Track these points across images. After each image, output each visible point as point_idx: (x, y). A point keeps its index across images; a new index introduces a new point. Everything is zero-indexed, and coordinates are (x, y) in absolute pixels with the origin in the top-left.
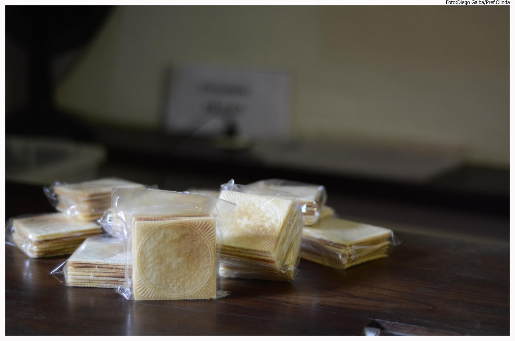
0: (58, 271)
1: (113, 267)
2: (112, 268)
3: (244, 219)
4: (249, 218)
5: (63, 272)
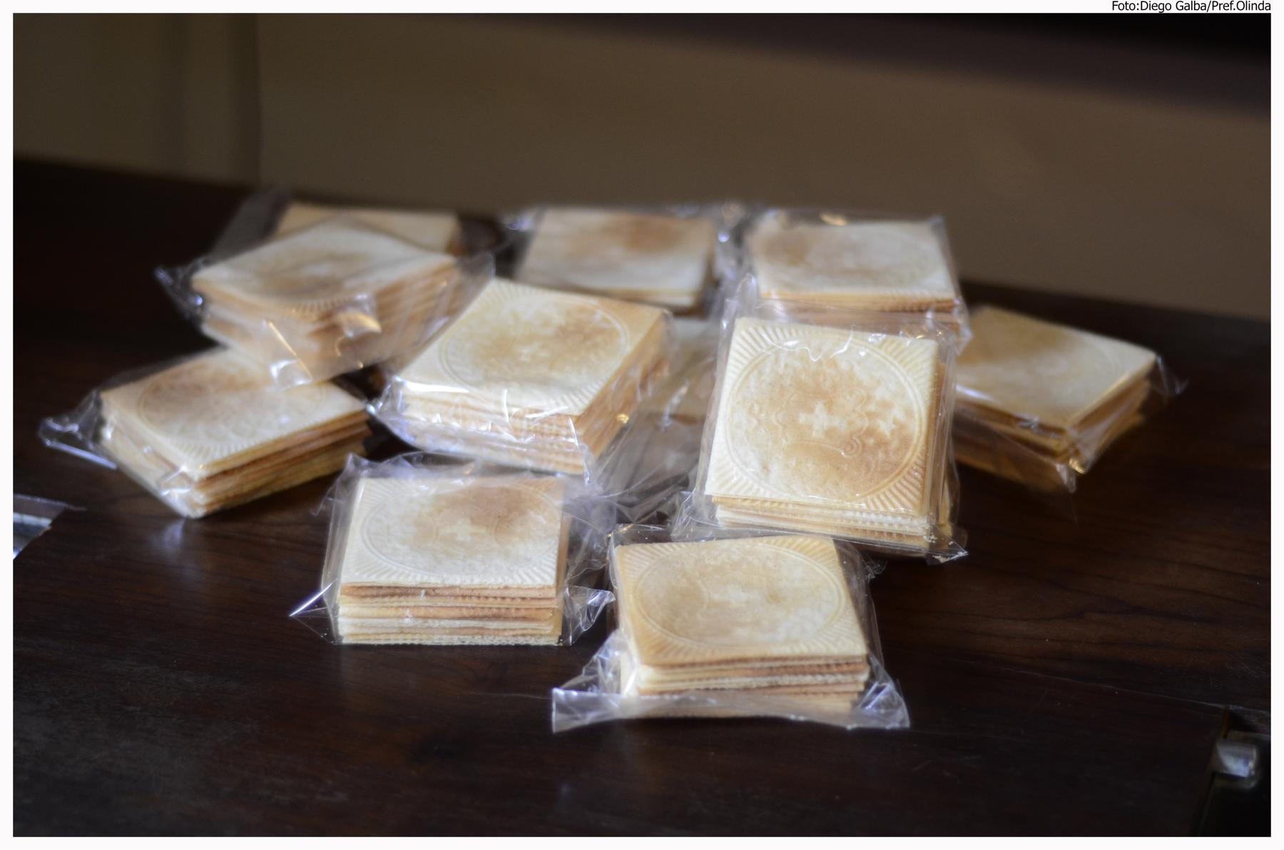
0: (311, 607)
2: (464, 597)
3: (817, 411)
4: (830, 406)
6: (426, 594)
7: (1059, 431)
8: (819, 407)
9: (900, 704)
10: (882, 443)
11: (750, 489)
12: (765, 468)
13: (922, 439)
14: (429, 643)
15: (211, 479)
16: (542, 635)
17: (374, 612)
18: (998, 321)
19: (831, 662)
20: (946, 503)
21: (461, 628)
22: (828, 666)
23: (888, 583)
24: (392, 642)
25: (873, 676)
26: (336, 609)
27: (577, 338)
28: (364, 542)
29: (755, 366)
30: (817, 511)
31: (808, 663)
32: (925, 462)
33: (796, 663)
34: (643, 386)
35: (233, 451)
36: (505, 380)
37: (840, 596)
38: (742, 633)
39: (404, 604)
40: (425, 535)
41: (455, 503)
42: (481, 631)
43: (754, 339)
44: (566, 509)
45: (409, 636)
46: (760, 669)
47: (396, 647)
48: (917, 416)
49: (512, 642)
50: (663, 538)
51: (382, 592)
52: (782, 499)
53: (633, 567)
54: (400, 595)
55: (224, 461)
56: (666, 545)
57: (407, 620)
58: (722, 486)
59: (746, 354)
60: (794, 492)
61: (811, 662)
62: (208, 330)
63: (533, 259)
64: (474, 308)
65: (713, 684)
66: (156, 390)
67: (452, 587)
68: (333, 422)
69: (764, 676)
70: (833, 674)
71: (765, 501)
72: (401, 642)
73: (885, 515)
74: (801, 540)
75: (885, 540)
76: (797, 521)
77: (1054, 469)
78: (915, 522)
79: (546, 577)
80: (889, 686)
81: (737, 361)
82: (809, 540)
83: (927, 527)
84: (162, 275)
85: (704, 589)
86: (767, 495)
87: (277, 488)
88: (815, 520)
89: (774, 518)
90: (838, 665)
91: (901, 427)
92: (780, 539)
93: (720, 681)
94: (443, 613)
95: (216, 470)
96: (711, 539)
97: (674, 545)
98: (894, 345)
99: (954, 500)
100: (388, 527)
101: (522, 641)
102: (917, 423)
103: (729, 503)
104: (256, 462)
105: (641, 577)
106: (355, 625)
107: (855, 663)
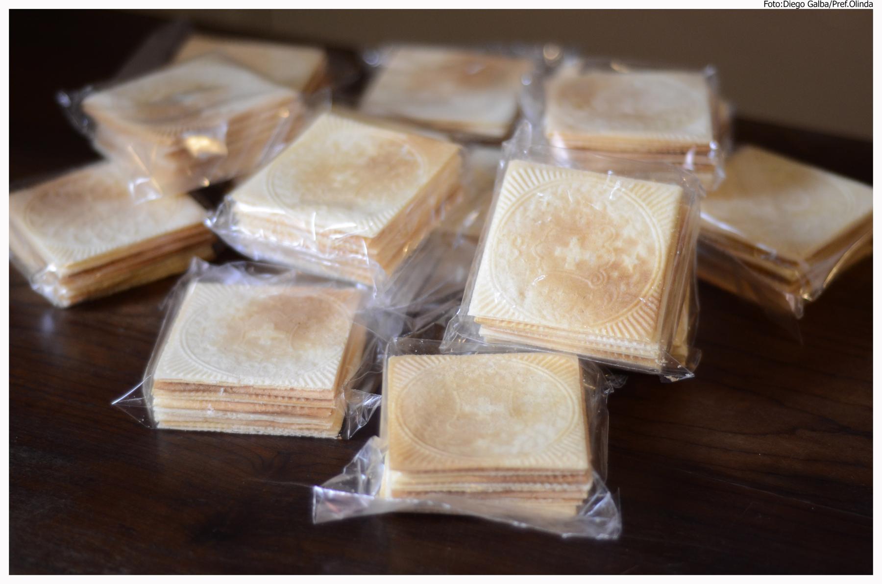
0: (130, 396)
1: (260, 392)
2: (257, 395)
3: (572, 245)
5: (143, 401)
6: (225, 391)
7: (793, 264)
8: (574, 241)
9: (614, 515)
10: (624, 277)
11: (507, 312)
12: (522, 294)
13: (660, 274)
14: (229, 431)
15: (73, 277)
16: (324, 430)
17: (183, 404)
18: (757, 161)
19: (557, 473)
20: (684, 325)
21: (256, 421)
22: (555, 477)
23: (622, 401)
24: (199, 429)
25: (593, 491)
26: (151, 399)
27: (384, 167)
28: (181, 342)
29: (522, 203)
30: (564, 333)
31: (537, 473)
32: (661, 295)
33: (526, 473)
34: (438, 211)
35: (93, 254)
36: (316, 204)
37: (574, 413)
38: (481, 443)
39: (207, 398)
40: (234, 339)
41: (264, 309)
42: (272, 424)
43: (524, 180)
44: (357, 318)
45: (212, 425)
46: (496, 477)
47: (202, 433)
48: (657, 253)
49: (299, 434)
50: (433, 350)
51: (188, 388)
52: (534, 322)
53: (402, 374)
54: (204, 391)
55: (85, 262)
56: (433, 357)
57: (209, 412)
58: (483, 308)
59: (515, 193)
60: (544, 317)
61: (540, 473)
62: (98, 145)
63: (378, 94)
64: (304, 138)
65: (455, 487)
66: (44, 197)
67: (246, 387)
68: (182, 230)
69: (498, 482)
70: (560, 483)
71: (519, 323)
72: (206, 429)
73: (622, 340)
74: (550, 357)
75: (623, 360)
76: (549, 341)
77: (784, 298)
78: (648, 348)
79: (326, 381)
80: (608, 496)
81: (507, 198)
82: (557, 358)
83: (658, 352)
84: (64, 100)
85: (458, 400)
86: (521, 319)
87: (135, 282)
88: (562, 341)
89: (528, 337)
90: (564, 476)
91: (643, 262)
92: (533, 355)
93: (460, 485)
94: (239, 407)
95: (76, 270)
96: (473, 353)
97: (440, 357)
98: (644, 189)
99: (692, 326)
100: (204, 329)
101: (307, 434)
102: (657, 259)
103: (489, 323)
104: (112, 262)
105: (406, 386)
106: (167, 414)
107: (577, 475)
